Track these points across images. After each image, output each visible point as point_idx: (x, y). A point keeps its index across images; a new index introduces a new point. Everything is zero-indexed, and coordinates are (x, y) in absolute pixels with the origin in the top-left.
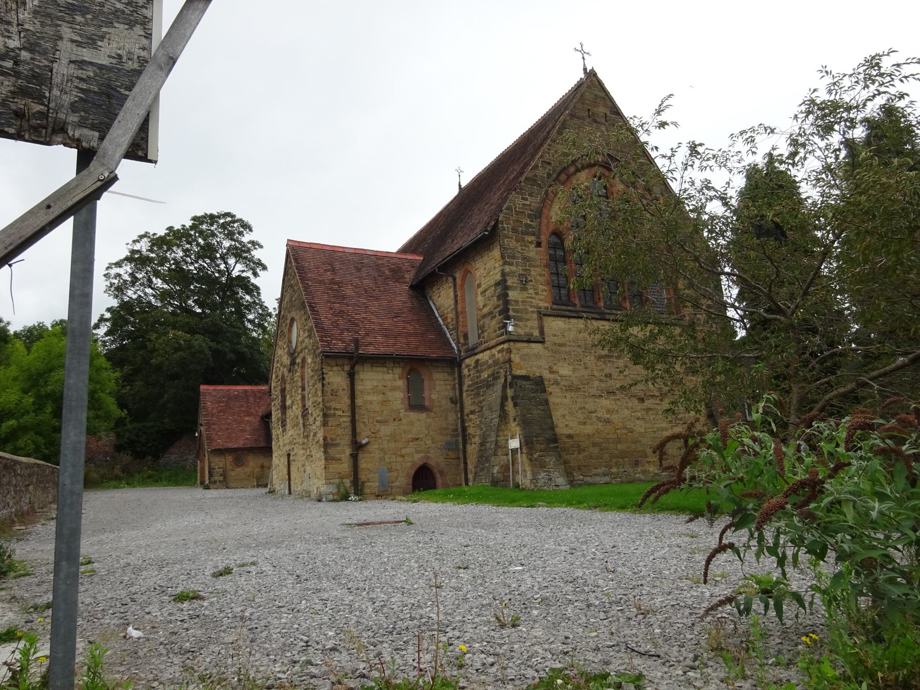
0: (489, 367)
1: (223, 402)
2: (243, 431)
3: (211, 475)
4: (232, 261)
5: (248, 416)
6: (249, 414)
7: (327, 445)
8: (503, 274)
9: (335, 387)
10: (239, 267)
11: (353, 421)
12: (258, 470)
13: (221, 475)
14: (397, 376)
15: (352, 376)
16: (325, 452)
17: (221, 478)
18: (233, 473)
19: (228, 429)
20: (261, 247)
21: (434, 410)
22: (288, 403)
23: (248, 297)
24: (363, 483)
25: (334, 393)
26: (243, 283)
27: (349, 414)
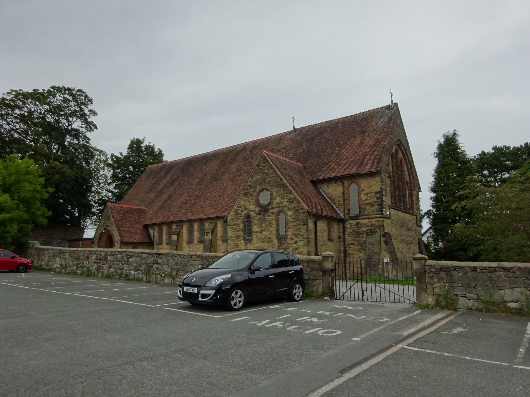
0: (368, 226)
1: (121, 214)
2: (136, 232)
6: (137, 223)
8: (381, 189)
15: (315, 224)
22: (255, 228)
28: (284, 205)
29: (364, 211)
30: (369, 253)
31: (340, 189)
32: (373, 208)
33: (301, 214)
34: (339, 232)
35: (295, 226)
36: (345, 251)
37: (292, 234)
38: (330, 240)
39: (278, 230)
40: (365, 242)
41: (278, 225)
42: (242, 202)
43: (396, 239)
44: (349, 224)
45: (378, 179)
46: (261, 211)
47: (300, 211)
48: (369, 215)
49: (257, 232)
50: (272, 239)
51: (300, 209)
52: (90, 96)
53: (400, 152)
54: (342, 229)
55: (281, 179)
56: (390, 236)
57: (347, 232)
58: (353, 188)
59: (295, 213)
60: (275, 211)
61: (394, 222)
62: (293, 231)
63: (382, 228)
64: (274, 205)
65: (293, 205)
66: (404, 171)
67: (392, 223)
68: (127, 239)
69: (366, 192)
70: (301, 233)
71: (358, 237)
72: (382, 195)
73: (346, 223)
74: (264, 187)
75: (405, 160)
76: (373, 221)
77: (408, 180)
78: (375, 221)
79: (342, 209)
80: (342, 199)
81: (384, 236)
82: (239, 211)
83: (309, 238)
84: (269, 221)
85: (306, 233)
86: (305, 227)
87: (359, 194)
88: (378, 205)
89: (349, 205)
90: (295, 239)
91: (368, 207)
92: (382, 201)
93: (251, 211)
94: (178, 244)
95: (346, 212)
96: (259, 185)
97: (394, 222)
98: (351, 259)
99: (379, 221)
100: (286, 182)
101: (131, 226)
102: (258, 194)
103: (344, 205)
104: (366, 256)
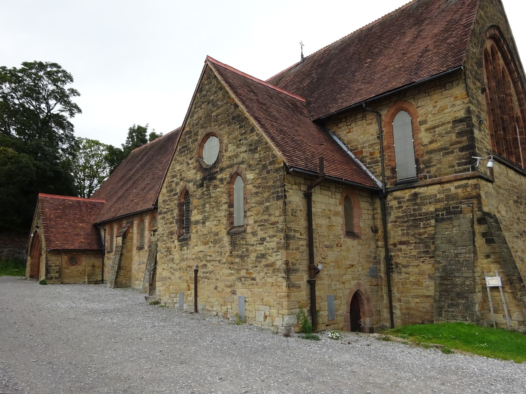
1: (59, 209)
2: (78, 235)
3: (47, 272)
4: (52, 102)
5: (81, 223)
6: (83, 221)
7: (289, 270)
9: (294, 207)
10: (59, 106)
11: (310, 245)
12: (90, 268)
13: (57, 272)
14: (338, 201)
15: (308, 197)
16: (288, 279)
17: (57, 275)
18: (67, 271)
19: (64, 233)
20: (79, 95)
21: (362, 237)
22: (195, 216)
23: (61, 132)
24: (318, 311)
25: (294, 213)
26: (59, 121)
27: (305, 237)
28: (240, 160)
29: (427, 167)
30: (444, 263)
31: (374, 129)
32: (450, 158)
33: (271, 176)
34: (374, 218)
35: (261, 203)
36: (388, 259)
37: (255, 222)
38: (350, 234)
39: (230, 215)
40: (433, 238)
41: (231, 205)
42: (178, 167)
43: (509, 230)
44: (395, 198)
45: (459, 90)
46: (204, 179)
47: (269, 168)
48: (440, 175)
49: (197, 222)
50: (220, 235)
51: (270, 164)
52: (68, 71)
53: (499, 54)
54: (379, 211)
55: (236, 106)
56: (497, 221)
57: (391, 218)
58: (402, 121)
59: (260, 174)
60: (225, 175)
61: (501, 191)
62: (257, 215)
63: (475, 201)
64: (225, 163)
65: (257, 156)
66: (511, 95)
67: (498, 193)
68: (58, 244)
69: (429, 124)
70: (273, 219)
71: (417, 227)
72: (471, 126)
73: (389, 197)
74: (209, 130)
75: (511, 73)
76: (452, 188)
77: (519, 114)
78: (457, 187)
79: (379, 169)
80: (378, 147)
81: (481, 221)
82: (174, 185)
83: (290, 229)
84: (216, 197)
85: (282, 218)
86: (280, 203)
87: (415, 132)
88: (461, 150)
89: (392, 158)
90: (261, 234)
91: (436, 157)
92: (472, 139)
93: (189, 181)
94: (124, 251)
95: (388, 173)
96: (202, 127)
97: (501, 191)
98: (403, 276)
99: (466, 186)
100: (245, 111)
101: (71, 226)
102: (201, 146)
103: (383, 161)
104: (437, 269)
